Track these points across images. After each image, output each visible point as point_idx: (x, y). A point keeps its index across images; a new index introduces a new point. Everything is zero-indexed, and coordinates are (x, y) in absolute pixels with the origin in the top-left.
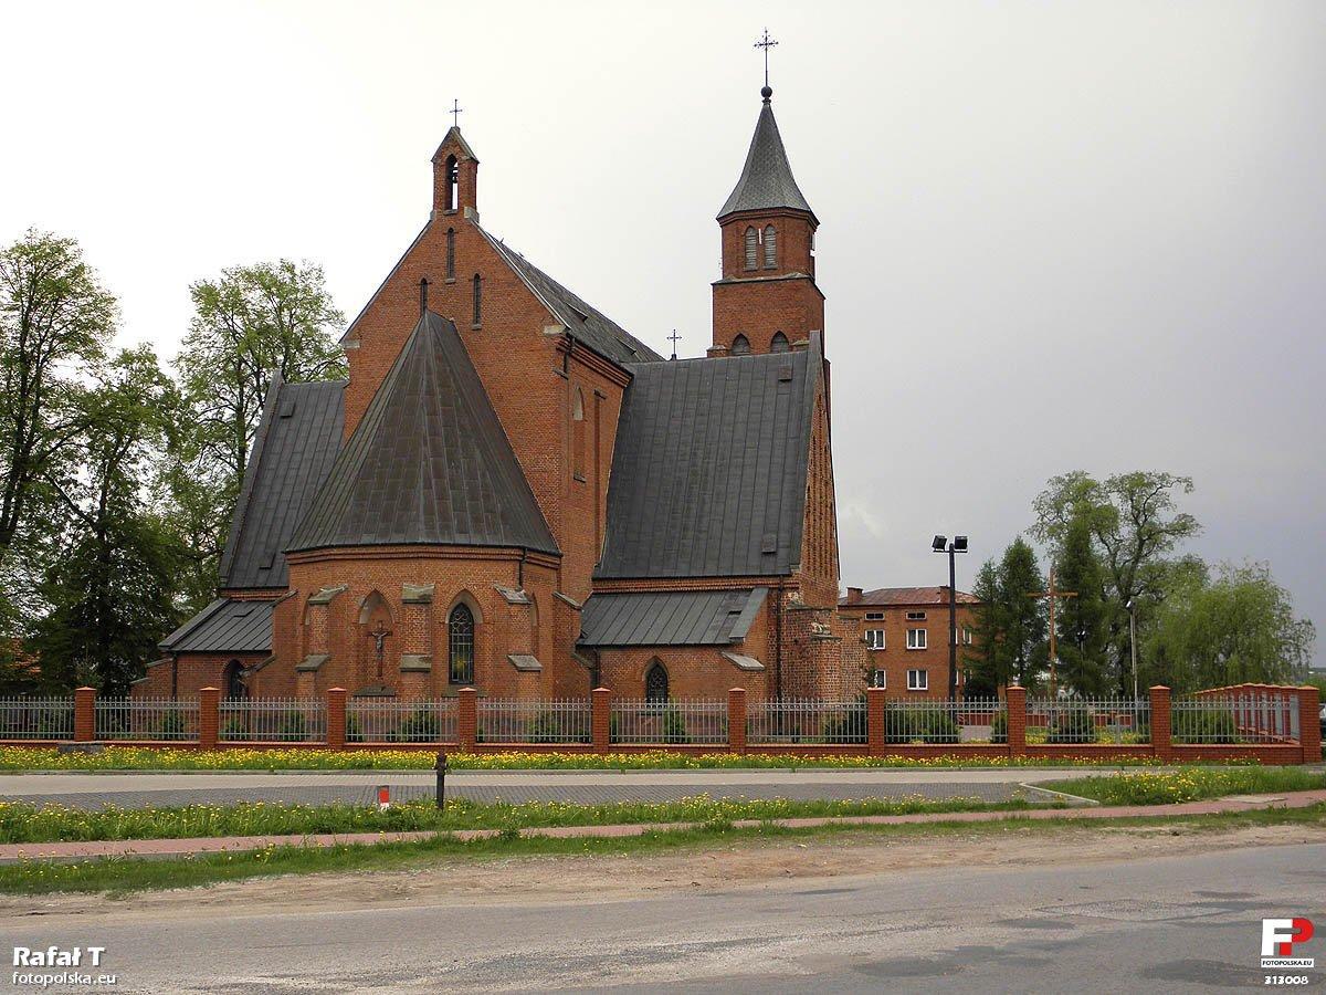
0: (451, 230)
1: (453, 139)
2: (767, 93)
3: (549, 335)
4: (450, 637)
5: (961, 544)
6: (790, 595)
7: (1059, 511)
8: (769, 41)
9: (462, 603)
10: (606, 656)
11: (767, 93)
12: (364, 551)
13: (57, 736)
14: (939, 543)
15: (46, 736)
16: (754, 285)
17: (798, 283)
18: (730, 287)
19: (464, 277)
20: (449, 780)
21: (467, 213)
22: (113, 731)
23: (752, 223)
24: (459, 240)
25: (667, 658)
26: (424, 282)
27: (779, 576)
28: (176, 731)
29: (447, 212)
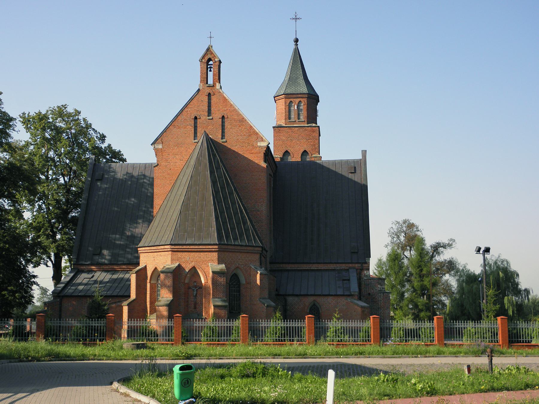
0: (209, 94)
1: (209, 50)
2: (296, 41)
3: (260, 146)
4: (230, 290)
5: (487, 250)
6: (365, 272)
7: (398, 237)
8: (298, 17)
9: (235, 274)
10: (290, 299)
11: (296, 41)
12: (188, 247)
13: (366, 340)
14: (479, 250)
15: (213, 339)
16: (293, 128)
17: (314, 128)
18: (282, 129)
19: (217, 116)
20: (496, 360)
21: (218, 86)
22: (154, 337)
23: (292, 100)
24: (214, 99)
25: (321, 300)
26: (196, 118)
27: (360, 263)
28: (213, 337)
29: (207, 85)
